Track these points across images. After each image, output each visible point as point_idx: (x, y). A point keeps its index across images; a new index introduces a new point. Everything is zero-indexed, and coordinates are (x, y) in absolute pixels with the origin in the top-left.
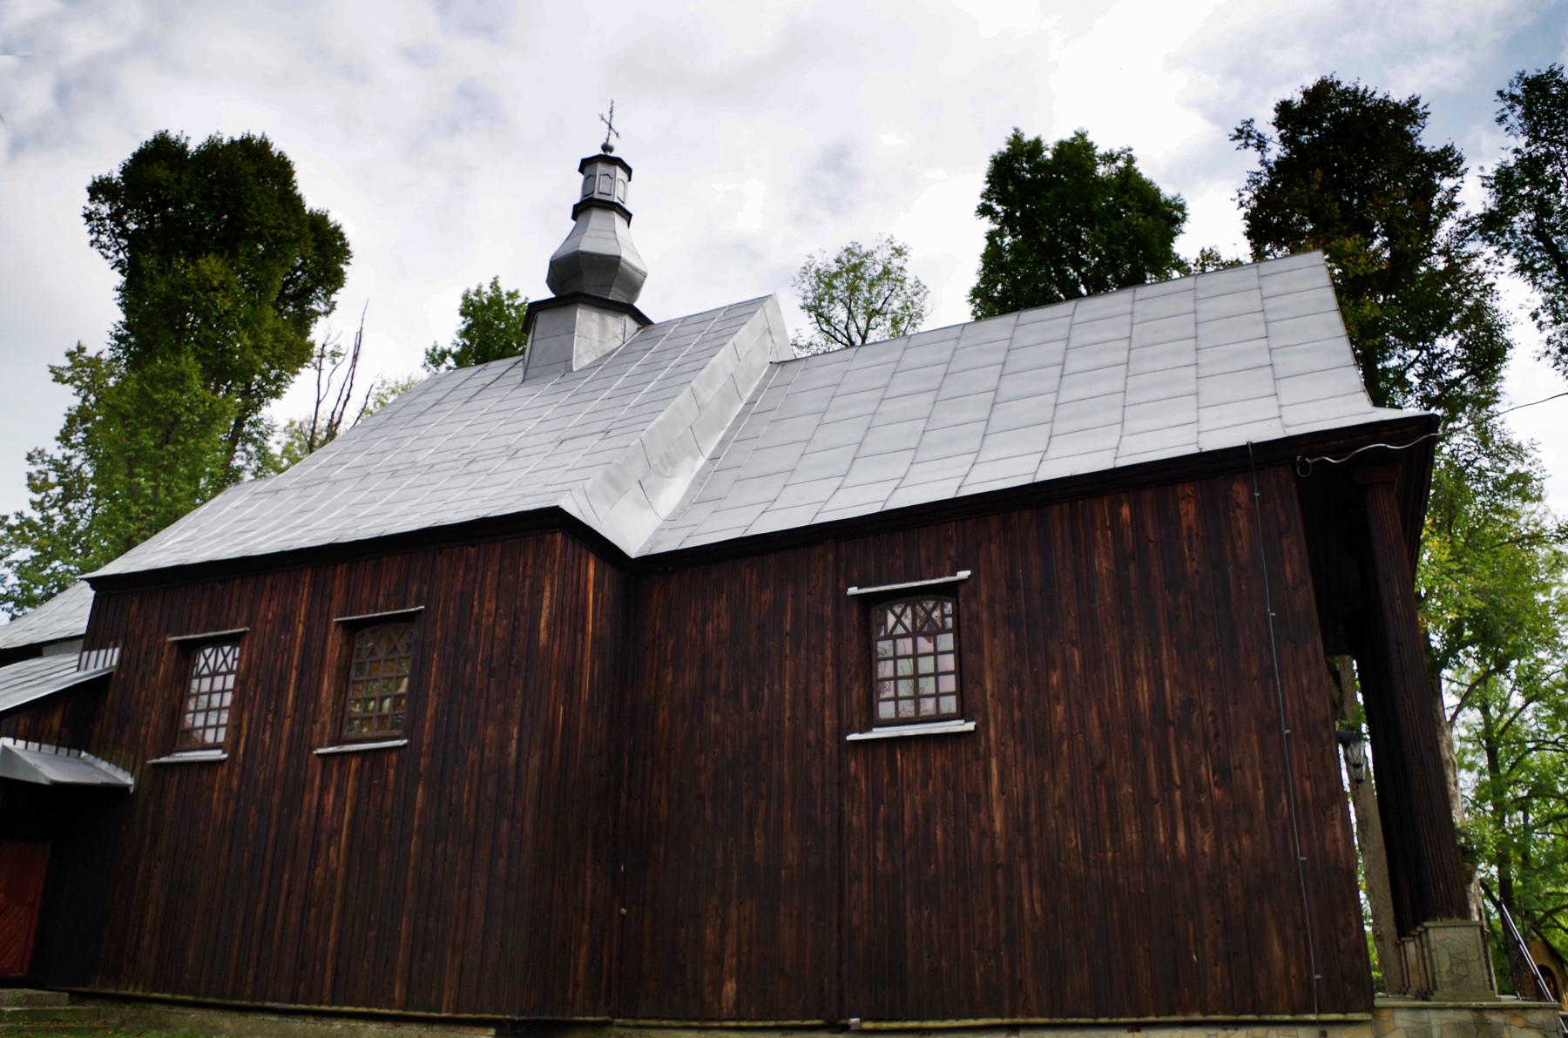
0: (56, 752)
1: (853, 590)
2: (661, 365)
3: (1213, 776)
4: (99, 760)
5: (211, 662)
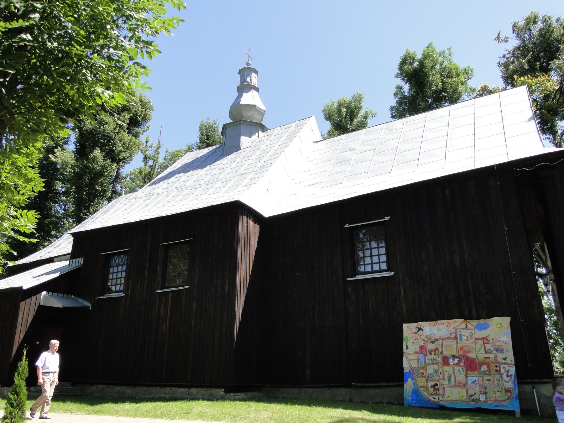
0: (63, 296)
1: (347, 226)
2: (273, 145)
3: (485, 290)
4: (78, 298)
5: (117, 261)
